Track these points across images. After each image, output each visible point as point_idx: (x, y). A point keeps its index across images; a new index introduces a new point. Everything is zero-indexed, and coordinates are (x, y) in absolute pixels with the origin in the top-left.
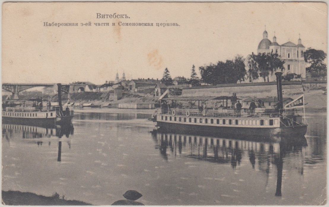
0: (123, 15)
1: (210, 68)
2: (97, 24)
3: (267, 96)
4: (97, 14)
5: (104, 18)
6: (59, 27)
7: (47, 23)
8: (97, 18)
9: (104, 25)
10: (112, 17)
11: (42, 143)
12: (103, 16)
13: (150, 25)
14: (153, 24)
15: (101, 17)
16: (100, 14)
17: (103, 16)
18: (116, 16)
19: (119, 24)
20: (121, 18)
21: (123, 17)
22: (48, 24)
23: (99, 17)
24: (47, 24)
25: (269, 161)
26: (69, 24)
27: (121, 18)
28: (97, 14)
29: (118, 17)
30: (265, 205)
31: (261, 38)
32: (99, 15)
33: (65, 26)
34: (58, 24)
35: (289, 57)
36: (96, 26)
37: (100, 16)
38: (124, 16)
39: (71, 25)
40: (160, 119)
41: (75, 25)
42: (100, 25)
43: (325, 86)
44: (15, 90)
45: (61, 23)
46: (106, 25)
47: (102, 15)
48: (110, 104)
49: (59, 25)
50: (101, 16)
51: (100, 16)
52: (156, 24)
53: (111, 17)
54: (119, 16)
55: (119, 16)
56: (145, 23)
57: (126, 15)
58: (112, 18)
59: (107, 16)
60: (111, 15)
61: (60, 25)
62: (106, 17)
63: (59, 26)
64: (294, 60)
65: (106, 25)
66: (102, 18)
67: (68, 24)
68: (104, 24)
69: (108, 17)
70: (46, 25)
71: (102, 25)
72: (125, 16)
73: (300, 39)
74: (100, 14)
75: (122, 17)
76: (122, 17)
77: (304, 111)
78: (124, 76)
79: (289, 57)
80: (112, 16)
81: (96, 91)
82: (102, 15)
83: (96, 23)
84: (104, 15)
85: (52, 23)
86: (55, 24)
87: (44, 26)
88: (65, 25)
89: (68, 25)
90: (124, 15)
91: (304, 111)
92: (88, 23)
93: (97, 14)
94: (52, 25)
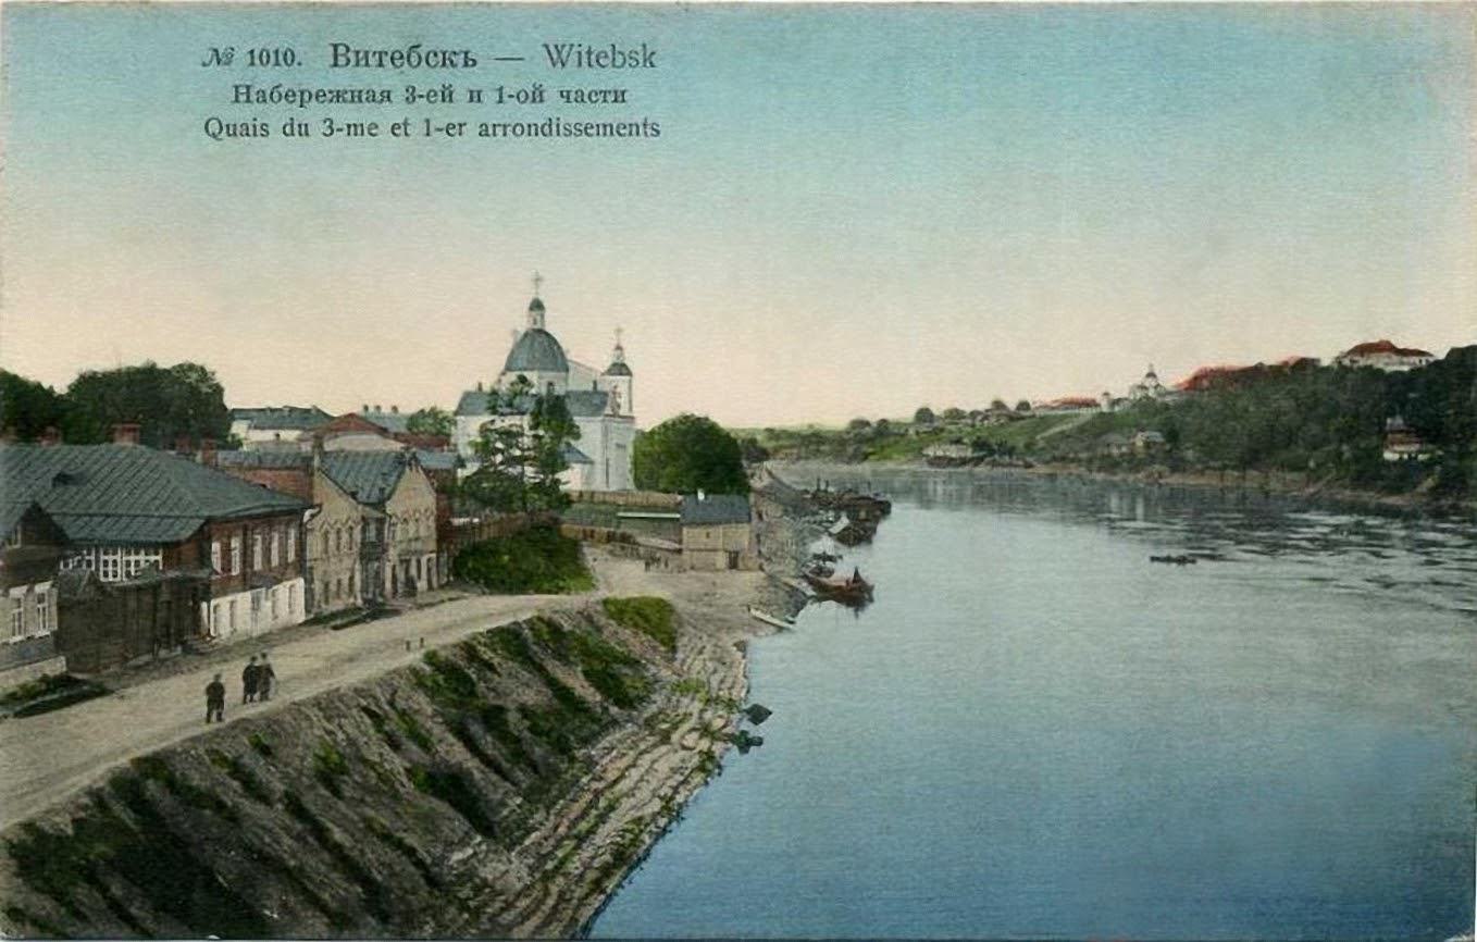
3: (785, 633)
4: (335, 47)
5: (367, 64)
7: (248, 87)
11: (759, 742)
12: (362, 58)
13: (378, 97)
14: (389, 92)
15: (353, 62)
16: (348, 49)
17: (362, 58)
19: (393, 128)
21: (452, 62)
22: (253, 97)
23: (342, 61)
26: (352, 92)
27: (444, 64)
28: (331, 49)
31: (523, 324)
32: (341, 50)
34: (302, 93)
35: (232, 603)
38: (460, 60)
39: (360, 101)
42: (586, 99)
44: (280, 558)
45: (314, 92)
46: (611, 98)
48: (662, 606)
49: (546, 129)
50: (351, 56)
53: (398, 63)
54: (436, 55)
55: (436, 55)
57: (466, 53)
60: (397, 55)
61: (310, 96)
62: (373, 61)
63: (302, 101)
66: (357, 64)
68: (601, 97)
69: (386, 60)
70: (243, 98)
71: (594, 99)
73: (619, 348)
74: (348, 49)
75: (448, 62)
80: (402, 57)
81: (419, 590)
82: (357, 53)
89: (344, 101)
92: (438, 88)
93: (335, 47)
94: (271, 98)
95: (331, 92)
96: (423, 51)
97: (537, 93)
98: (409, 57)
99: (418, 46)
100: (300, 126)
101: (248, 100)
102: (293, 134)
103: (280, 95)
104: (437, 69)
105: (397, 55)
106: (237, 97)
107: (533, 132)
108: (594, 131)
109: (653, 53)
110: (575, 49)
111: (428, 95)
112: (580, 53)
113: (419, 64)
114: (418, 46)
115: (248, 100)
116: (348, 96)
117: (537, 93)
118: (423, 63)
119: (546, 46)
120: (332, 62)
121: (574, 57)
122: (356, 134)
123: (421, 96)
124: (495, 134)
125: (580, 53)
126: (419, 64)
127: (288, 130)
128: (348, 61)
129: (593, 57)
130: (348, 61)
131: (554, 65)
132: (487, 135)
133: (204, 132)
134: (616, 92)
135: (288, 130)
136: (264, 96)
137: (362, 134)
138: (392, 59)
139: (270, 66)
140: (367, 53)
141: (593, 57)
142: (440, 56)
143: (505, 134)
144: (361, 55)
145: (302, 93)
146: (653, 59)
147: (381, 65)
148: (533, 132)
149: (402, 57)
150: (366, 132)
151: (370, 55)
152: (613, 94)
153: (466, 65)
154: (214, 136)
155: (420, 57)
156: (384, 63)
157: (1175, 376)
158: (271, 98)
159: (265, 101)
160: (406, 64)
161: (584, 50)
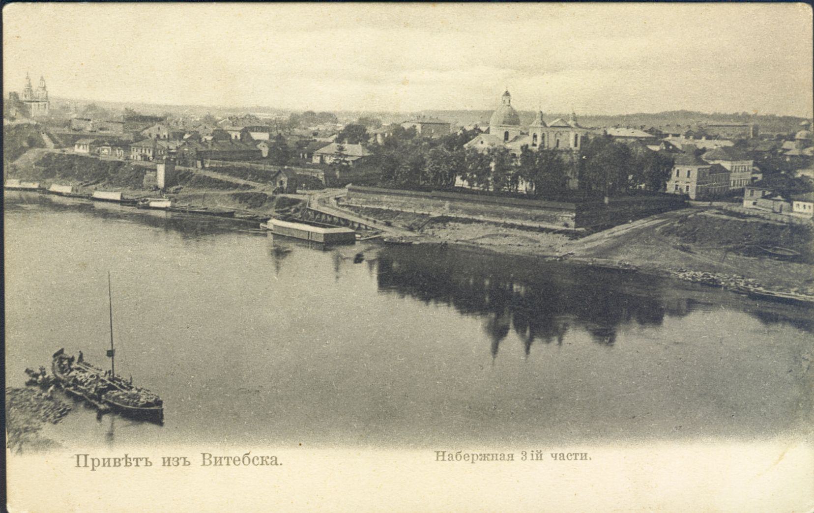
0: (268, 458)
2: (558, 456)
5: (221, 465)
6: (473, 462)
8: (204, 464)
15: (213, 463)
16: (210, 455)
18: (251, 462)
23: (207, 462)
24: (115, 463)
28: (162, 460)
29: (256, 462)
30: (415, 447)
32: (207, 456)
35: (689, 172)
36: (556, 459)
39: (109, 466)
42: (565, 458)
46: (579, 457)
49: (96, 462)
52: (550, 455)
53: (237, 463)
55: (258, 459)
57: (146, 459)
59: (228, 460)
60: (237, 459)
62: (224, 462)
64: (493, 196)
65: (579, 457)
68: (574, 457)
69: (231, 462)
72: (144, 460)
74: (210, 455)
75: (264, 462)
76: (264, 462)
78: (112, 431)
79: (689, 172)
80: (239, 460)
83: (556, 454)
84: (221, 458)
87: (204, 464)
88: (481, 460)
96: (251, 456)
97: (539, 455)
98: (243, 459)
99: (248, 454)
101: (496, 459)
103: (249, 459)
105: (237, 459)
113: (461, 459)
114: (248, 454)
115: (496, 459)
116: (490, 457)
117: (539, 455)
120: (202, 463)
126: (461, 459)
128: (211, 462)
130: (211, 462)
134: (582, 454)
136: (452, 457)
139: (100, 466)
142: (260, 459)
144: (106, 460)
145: (473, 455)
147: (228, 464)
149: (239, 460)
151: (223, 459)
152: (580, 455)
153: (184, 464)
155: (461, 457)
156: (230, 463)
157: (722, 113)
159: (564, 459)
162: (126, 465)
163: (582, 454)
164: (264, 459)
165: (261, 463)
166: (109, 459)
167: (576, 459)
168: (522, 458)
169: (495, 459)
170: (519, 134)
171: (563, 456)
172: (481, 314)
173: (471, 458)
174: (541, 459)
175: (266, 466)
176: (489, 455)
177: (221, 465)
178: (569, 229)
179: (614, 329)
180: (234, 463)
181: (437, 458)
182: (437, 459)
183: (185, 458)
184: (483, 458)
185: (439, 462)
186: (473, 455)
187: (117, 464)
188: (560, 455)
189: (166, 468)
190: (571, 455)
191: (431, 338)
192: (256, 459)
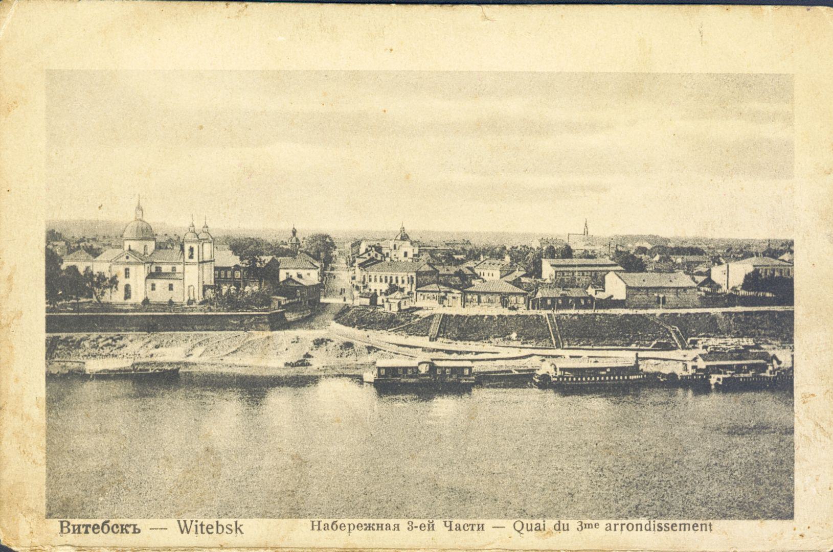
1: (791, 519)
9: (86, 532)
10: (100, 530)
13: (392, 528)
14: (398, 525)
15: (72, 531)
18: (111, 530)
20: (122, 532)
21: (127, 532)
23: (65, 530)
25: (78, 303)
26: (378, 525)
27: (122, 532)
29: (115, 530)
33: (367, 532)
36: (451, 530)
37: (69, 527)
38: (131, 529)
39: (382, 529)
40: (521, 398)
41: (392, 528)
42: (462, 528)
43: (48, 334)
46: (476, 528)
47: (74, 526)
49: (352, 527)
51: (69, 527)
55: (117, 527)
56: (122, 526)
58: (98, 533)
62: (83, 530)
66: (74, 532)
67: (374, 524)
69: (90, 530)
70: (316, 528)
71: (466, 528)
72: (132, 527)
76: (124, 531)
77: (48, 314)
85: (104, 524)
86: (358, 527)
88: (366, 529)
89: (127, 532)
90: (131, 525)
91: (48, 314)
95: (365, 524)
97: (431, 526)
100: (563, 524)
102: (650, 530)
103: (337, 526)
104: (119, 534)
106: (319, 524)
107: (639, 529)
108: (678, 528)
109: (241, 526)
110: (194, 523)
111: (421, 526)
112: (196, 526)
116: (375, 527)
117: (431, 526)
118: (356, 528)
119: (711, 530)
120: (311, 528)
121: (193, 528)
122: (685, 530)
123: (416, 527)
124: (615, 530)
125: (196, 526)
126: (632, 529)
127: (557, 527)
128: (69, 530)
129: (204, 528)
130: (69, 530)
131: (182, 532)
132: (540, 530)
133: (513, 528)
134: (479, 525)
135: (557, 527)
137: (641, 530)
138: (93, 529)
139: (584, 529)
140: (378, 529)
141: (204, 528)
142: (120, 527)
143: (622, 530)
144: (76, 527)
145: (349, 525)
146: (241, 528)
148: (639, 529)
150: (643, 529)
151: (81, 527)
152: (477, 526)
153: (134, 532)
154: (519, 531)
156: (89, 531)
158: (633, 526)
160: (101, 531)
161: (199, 524)
162: (134, 532)
163: (479, 525)
164: (124, 527)
165: (120, 531)
166: (382, 525)
167: (472, 529)
168: (408, 528)
169: (380, 529)
170: (688, 291)
171: (328, 526)
172: (440, 396)
173: (347, 527)
174: (433, 529)
175: (125, 534)
176: (374, 524)
177: (79, 532)
178: (762, 351)
179: (266, 392)
180: (694, 529)
181: (313, 527)
182: (313, 529)
183: (135, 525)
184: (368, 528)
185: (452, 532)
186: (349, 525)
187: (396, 526)
188: (386, 525)
189: (316, 532)
190: (468, 526)
191: (603, 423)
192: (115, 527)
